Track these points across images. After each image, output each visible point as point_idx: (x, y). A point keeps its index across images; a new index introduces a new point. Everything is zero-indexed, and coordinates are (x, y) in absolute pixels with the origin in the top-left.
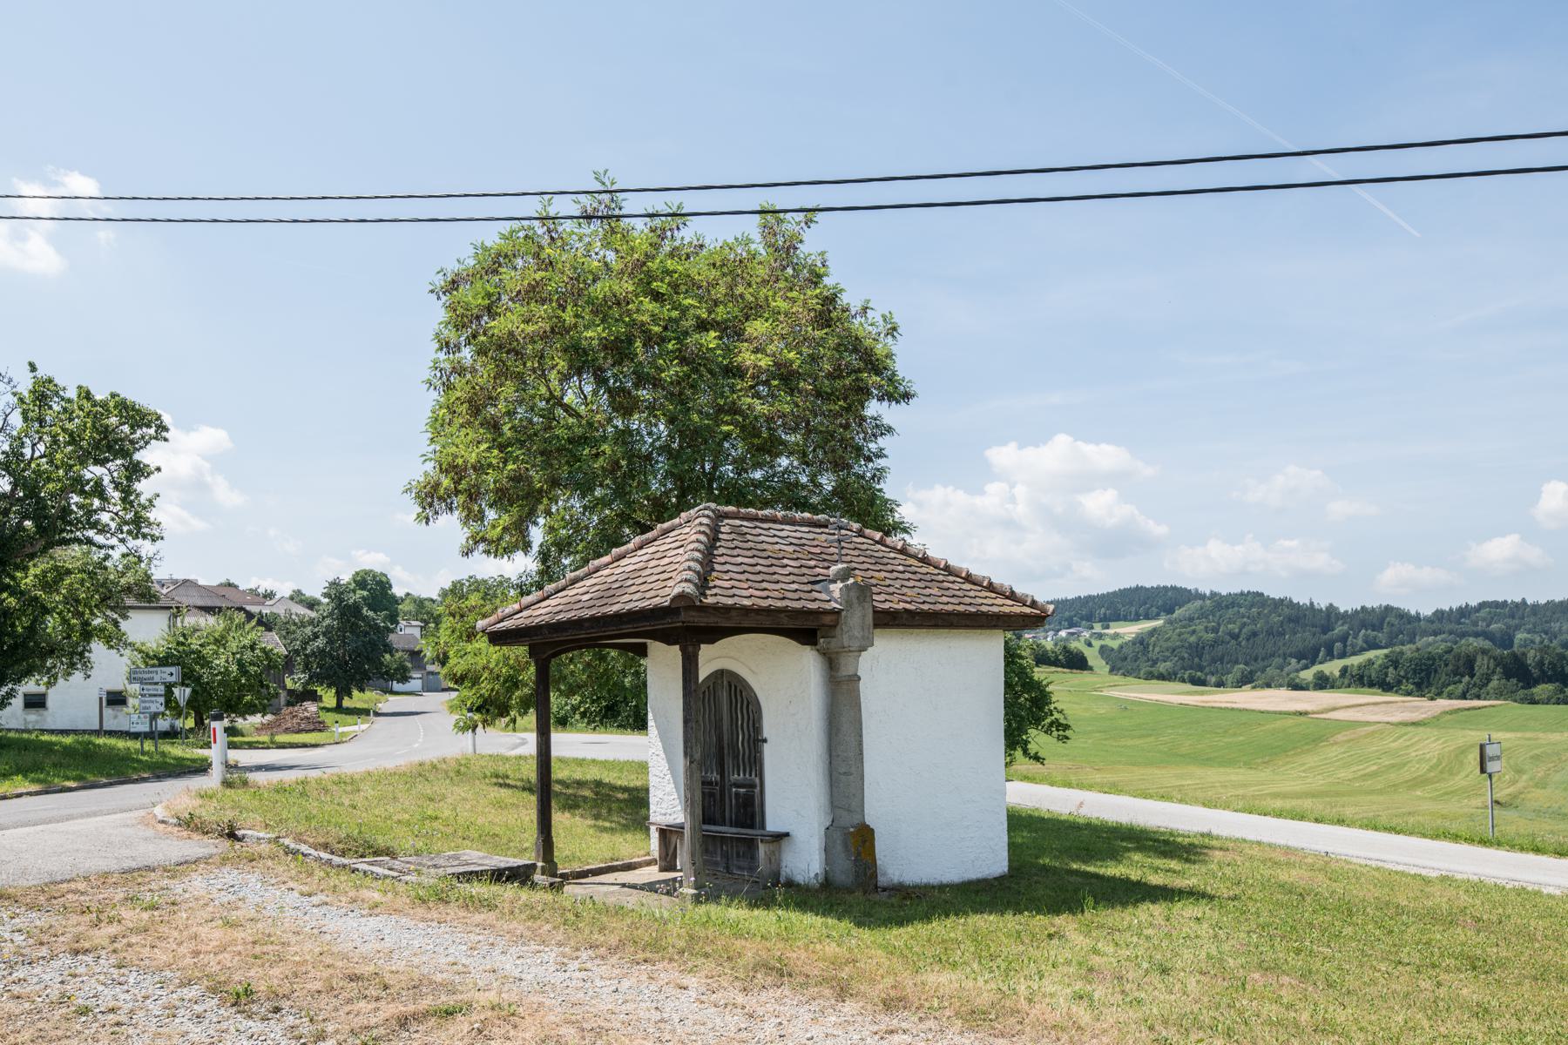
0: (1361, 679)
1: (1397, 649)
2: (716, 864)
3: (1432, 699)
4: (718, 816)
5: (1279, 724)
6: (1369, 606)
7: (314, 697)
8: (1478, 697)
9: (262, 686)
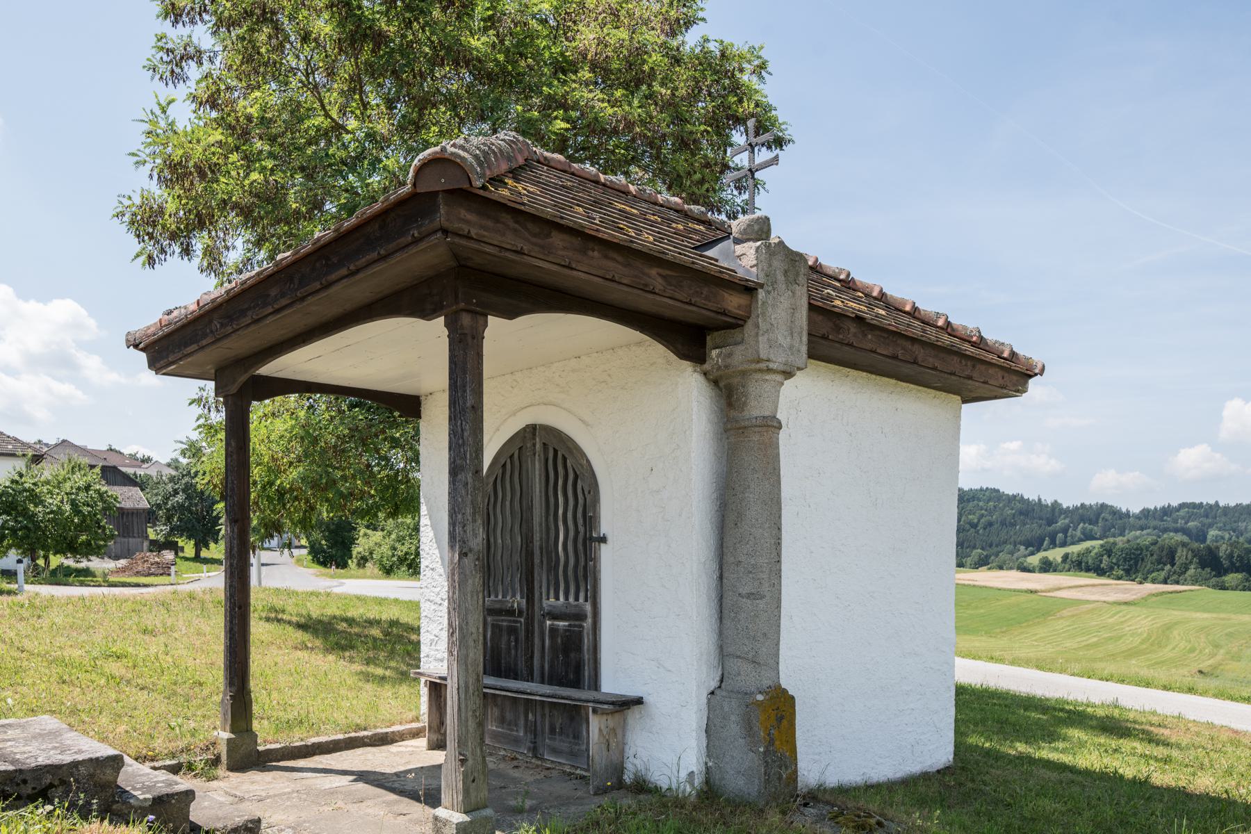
0: (1080, 565)
1: (1111, 540)
2: (517, 741)
3: (1141, 583)
4: (521, 664)
5: (1013, 600)
6: (1087, 503)
7: (174, 547)
8: (1177, 583)
9: (99, 527)
